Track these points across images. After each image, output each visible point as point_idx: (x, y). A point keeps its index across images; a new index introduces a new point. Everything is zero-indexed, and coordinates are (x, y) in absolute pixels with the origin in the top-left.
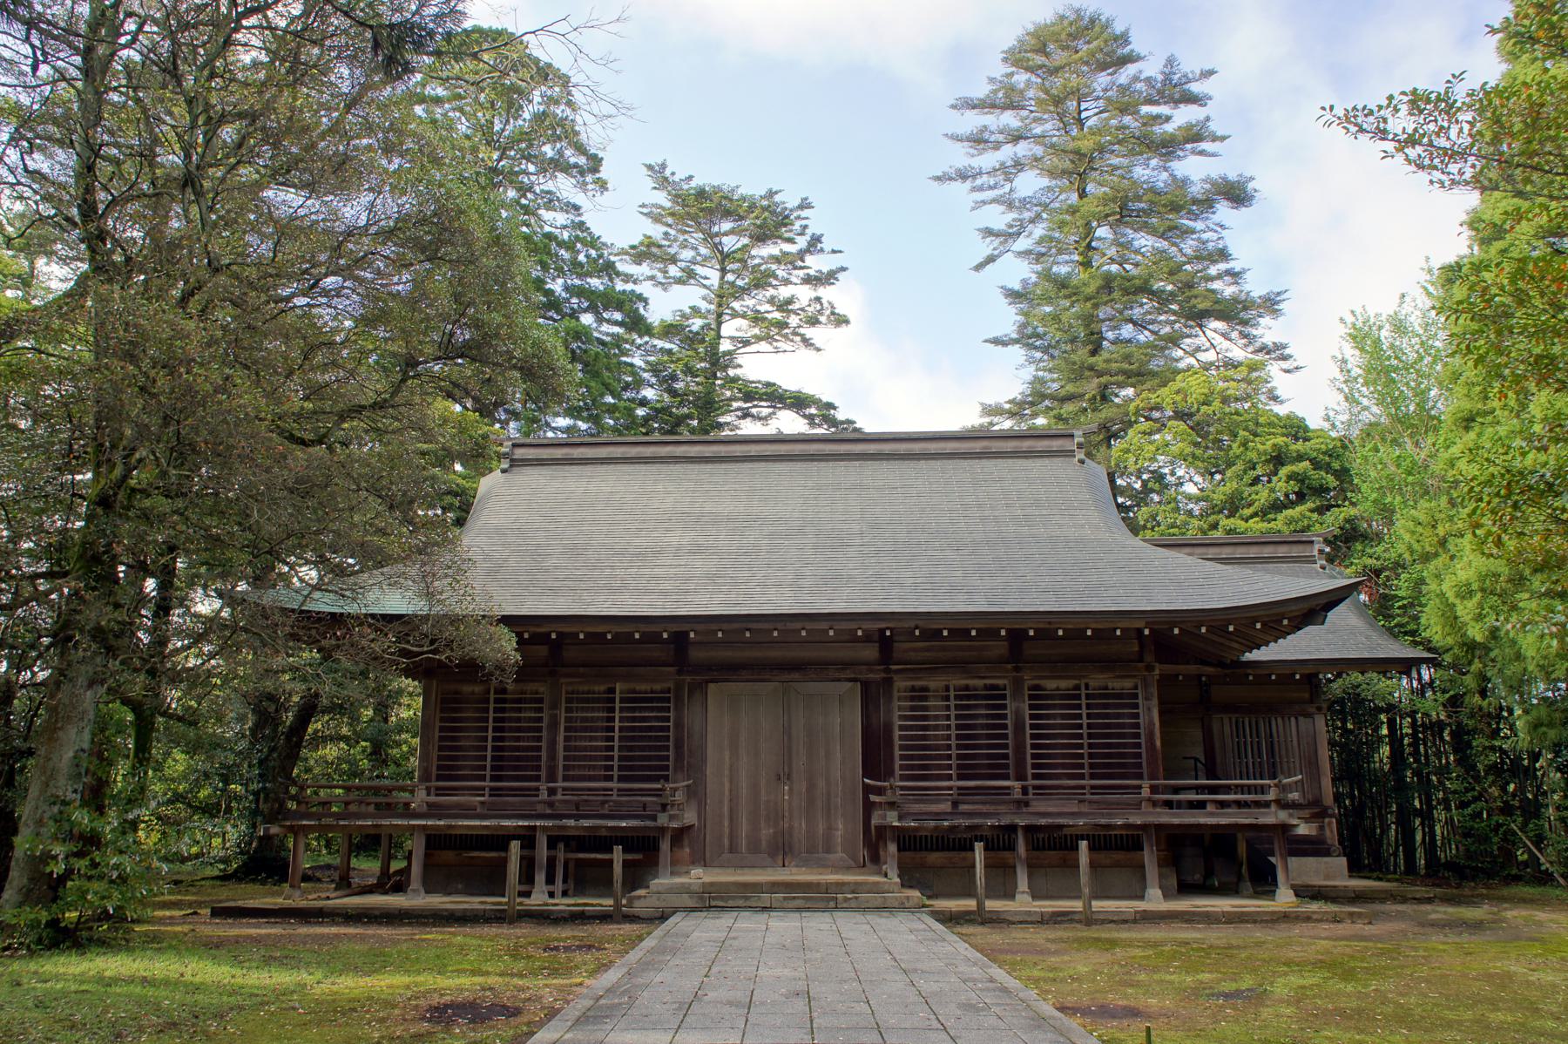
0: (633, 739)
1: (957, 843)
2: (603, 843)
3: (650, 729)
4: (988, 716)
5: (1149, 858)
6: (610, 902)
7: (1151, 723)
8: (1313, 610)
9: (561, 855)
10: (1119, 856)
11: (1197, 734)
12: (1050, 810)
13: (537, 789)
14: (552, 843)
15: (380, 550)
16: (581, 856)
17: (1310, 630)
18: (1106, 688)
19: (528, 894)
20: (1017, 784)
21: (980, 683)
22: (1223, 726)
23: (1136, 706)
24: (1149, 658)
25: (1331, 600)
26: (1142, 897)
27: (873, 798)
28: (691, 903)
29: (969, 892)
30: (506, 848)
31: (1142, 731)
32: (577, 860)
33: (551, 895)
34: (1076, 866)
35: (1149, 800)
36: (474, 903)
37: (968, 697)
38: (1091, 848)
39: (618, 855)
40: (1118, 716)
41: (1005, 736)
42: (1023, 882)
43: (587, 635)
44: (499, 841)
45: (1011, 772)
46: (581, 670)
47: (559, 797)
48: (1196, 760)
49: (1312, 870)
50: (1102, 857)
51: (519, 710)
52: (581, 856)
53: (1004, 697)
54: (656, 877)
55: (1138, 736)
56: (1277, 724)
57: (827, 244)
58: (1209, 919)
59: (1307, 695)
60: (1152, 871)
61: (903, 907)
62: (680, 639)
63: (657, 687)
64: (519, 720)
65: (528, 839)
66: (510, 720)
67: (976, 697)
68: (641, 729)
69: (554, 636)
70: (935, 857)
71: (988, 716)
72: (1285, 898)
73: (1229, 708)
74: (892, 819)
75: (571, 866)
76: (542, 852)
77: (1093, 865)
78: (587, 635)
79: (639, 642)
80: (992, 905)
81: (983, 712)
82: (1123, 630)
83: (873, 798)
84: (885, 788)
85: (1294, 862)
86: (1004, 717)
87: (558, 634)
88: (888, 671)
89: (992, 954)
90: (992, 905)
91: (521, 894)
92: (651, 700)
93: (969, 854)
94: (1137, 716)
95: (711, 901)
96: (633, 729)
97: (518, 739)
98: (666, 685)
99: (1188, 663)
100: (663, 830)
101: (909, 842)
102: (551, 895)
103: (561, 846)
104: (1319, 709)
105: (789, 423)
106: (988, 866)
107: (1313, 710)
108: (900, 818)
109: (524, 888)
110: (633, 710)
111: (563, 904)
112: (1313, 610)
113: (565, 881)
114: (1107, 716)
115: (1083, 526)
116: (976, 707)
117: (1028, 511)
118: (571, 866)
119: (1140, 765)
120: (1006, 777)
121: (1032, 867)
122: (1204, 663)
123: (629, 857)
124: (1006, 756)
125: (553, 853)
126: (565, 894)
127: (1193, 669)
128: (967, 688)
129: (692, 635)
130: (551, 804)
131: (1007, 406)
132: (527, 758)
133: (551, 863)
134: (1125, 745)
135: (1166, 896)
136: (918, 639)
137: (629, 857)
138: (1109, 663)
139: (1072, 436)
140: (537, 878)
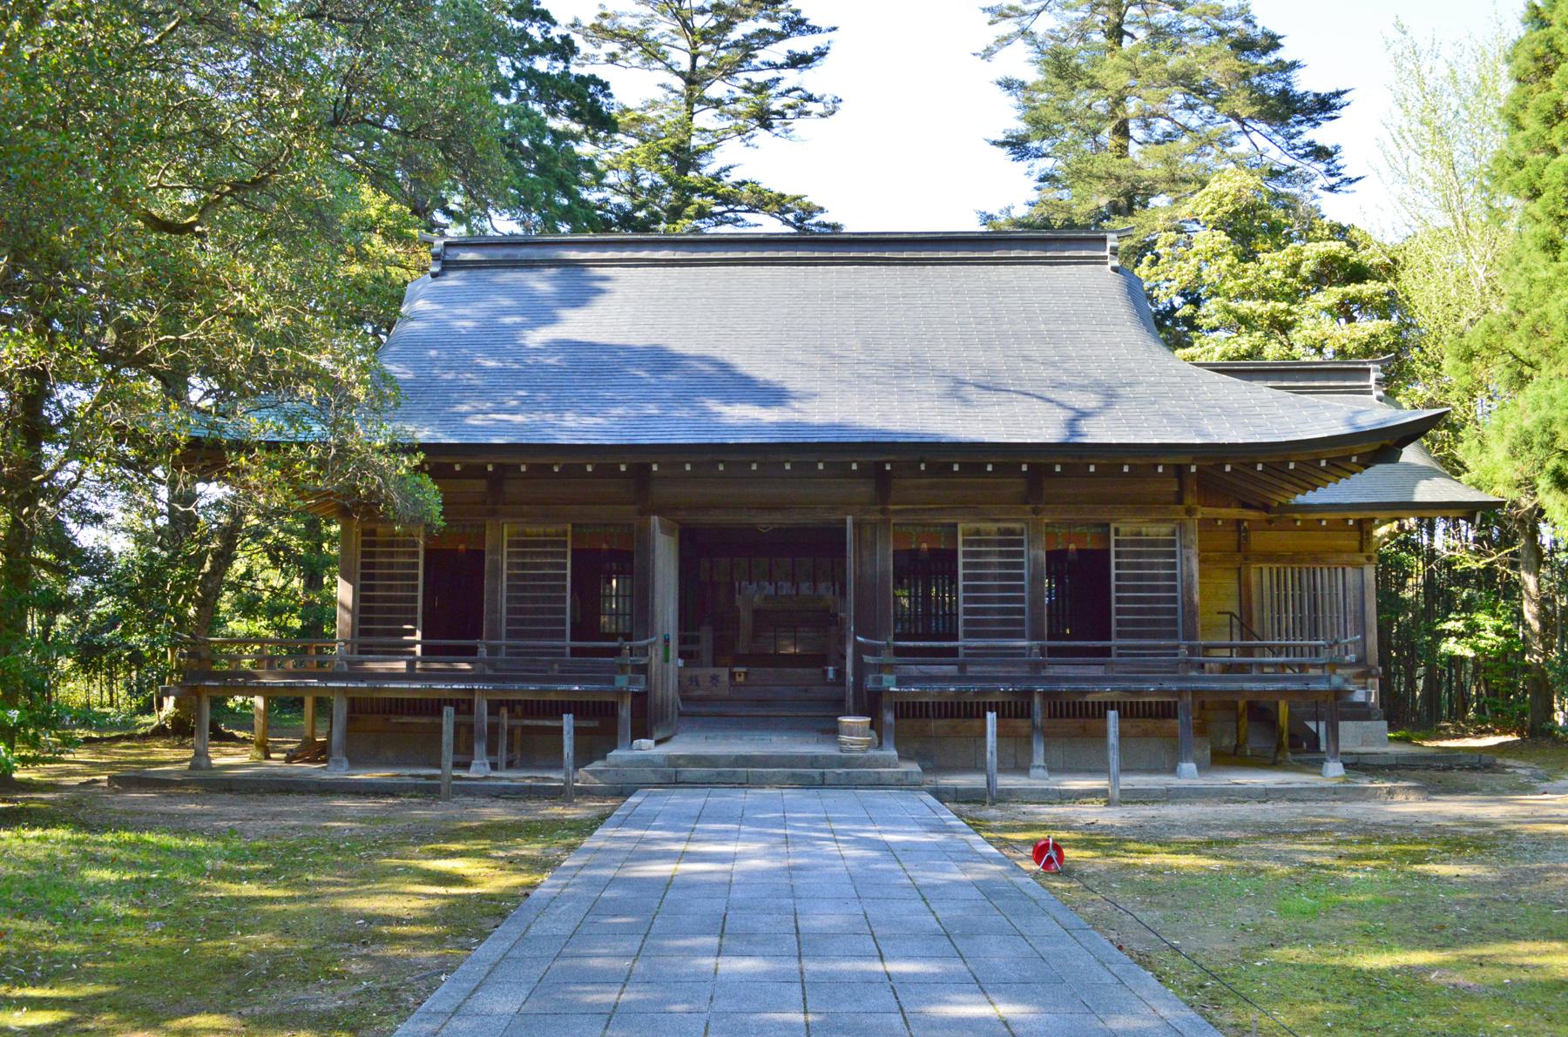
0: (524, 589)
2: (555, 709)
3: (544, 577)
4: (1001, 565)
6: (561, 776)
7: (1191, 575)
9: (505, 719)
10: (1149, 724)
13: (1177, 647)
14: (494, 708)
16: (527, 722)
17: (1379, 469)
18: (1139, 534)
19: (466, 766)
20: (1183, 643)
21: (993, 527)
23: (1173, 555)
24: (1189, 500)
26: (1173, 771)
27: (867, 659)
28: (654, 778)
29: (977, 766)
30: (440, 714)
31: (1178, 583)
32: (525, 728)
33: (494, 767)
34: (1103, 734)
35: (1187, 662)
36: (406, 774)
37: (979, 543)
38: (1122, 716)
39: (568, 721)
40: (1151, 566)
41: (1021, 588)
42: (1039, 758)
43: (530, 467)
44: (432, 707)
45: (1026, 628)
46: (525, 508)
47: (503, 656)
48: (1232, 614)
49: (1353, 736)
50: (1128, 723)
51: (391, 555)
52: (527, 722)
53: (1020, 543)
54: (614, 747)
55: (1173, 589)
56: (1323, 576)
57: (600, 11)
58: (1248, 795)
59: (1356, 544)
61: (903, 784)
62: (640, 472)
63: (551, 530)
64: (391, 566)
65: (463, 705)
66: (381, 566)
67: (987, 543)
68: (534, 578)
69: (490, 468)
70: (934, 725)
71: (1001, 565)
72: (1334, 769)
73: (1269, 557)
75: (518, 732)
77: (1122, 735)
78: (530, 467)
79: (525, 476)
80: (1006, 781)
81: (995, 560)
82: (1131, 466)
83: (867, 659)
84: (882, 647)
86: (1020, 566)
87: (496, 466)
88: (883, 512)
90: (1006, 781)
91: (456, 765)
92: (545, 544)
93: (977, 723)
94: (1173, 566)
95: (672, 777)
96: (523, 577)
97: (390, 588)
98: (560, 528)
99: (1228, 506)
100: (621, 693)
102: (494, 767)
103: (504, 711)
104: (1369, 558)
105: (768, 224)
106: (1000, 735)
107: (1363, 560)
108: (900, 682)
109: (461, 758)
110: (523, 555)
113: (510, 749)
114: (1139, 566)
115: (1117, 345)
116: (988, 554)
117: (1051, 327)
118: (518, 732)
119: (1174, 623)
120: (1021, 636)
122: (1246, 505)
123: (583, 724)
124: (1021, 611)
125: (494, 719)
126: (510, 765)
127: (1234, 512)
128: (978, 532)
129: (655, 468)
130: (492, 665)
132: (400, 610)
133: (494, 729)
134: (1158, 600)
135: (1201, 769)
136: (921, 475)
137: (583, 724)
139: (1104, 240)
140: (476, 747)
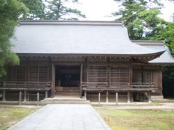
1: (96, 93)
5: (129, 95)
8: (158, 55)
11: (141, 75)
12: (113, 88)
15: (20, 114)
22: (145, 73)
25: (161, 53)
36: (61, 64)
44: (18, 92)
60: (129, 99)
65: (23, 92)
72: (150, 102)
74: (85, 89)
76: (25, 94)
77: (101, 97)
85: (152, 97)
89: (97, 109)
90: (101, 103)
101: (89, 93)
111: (29, 102)
112: (158, 55)
121: (109, 98)
131: (114, 18)
138: (124, 63)
